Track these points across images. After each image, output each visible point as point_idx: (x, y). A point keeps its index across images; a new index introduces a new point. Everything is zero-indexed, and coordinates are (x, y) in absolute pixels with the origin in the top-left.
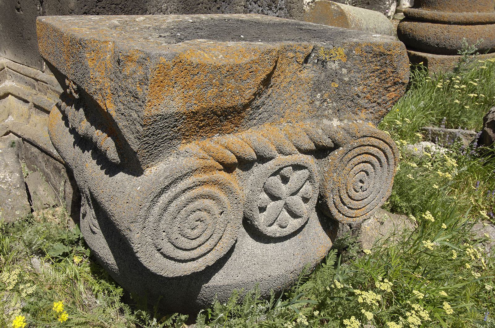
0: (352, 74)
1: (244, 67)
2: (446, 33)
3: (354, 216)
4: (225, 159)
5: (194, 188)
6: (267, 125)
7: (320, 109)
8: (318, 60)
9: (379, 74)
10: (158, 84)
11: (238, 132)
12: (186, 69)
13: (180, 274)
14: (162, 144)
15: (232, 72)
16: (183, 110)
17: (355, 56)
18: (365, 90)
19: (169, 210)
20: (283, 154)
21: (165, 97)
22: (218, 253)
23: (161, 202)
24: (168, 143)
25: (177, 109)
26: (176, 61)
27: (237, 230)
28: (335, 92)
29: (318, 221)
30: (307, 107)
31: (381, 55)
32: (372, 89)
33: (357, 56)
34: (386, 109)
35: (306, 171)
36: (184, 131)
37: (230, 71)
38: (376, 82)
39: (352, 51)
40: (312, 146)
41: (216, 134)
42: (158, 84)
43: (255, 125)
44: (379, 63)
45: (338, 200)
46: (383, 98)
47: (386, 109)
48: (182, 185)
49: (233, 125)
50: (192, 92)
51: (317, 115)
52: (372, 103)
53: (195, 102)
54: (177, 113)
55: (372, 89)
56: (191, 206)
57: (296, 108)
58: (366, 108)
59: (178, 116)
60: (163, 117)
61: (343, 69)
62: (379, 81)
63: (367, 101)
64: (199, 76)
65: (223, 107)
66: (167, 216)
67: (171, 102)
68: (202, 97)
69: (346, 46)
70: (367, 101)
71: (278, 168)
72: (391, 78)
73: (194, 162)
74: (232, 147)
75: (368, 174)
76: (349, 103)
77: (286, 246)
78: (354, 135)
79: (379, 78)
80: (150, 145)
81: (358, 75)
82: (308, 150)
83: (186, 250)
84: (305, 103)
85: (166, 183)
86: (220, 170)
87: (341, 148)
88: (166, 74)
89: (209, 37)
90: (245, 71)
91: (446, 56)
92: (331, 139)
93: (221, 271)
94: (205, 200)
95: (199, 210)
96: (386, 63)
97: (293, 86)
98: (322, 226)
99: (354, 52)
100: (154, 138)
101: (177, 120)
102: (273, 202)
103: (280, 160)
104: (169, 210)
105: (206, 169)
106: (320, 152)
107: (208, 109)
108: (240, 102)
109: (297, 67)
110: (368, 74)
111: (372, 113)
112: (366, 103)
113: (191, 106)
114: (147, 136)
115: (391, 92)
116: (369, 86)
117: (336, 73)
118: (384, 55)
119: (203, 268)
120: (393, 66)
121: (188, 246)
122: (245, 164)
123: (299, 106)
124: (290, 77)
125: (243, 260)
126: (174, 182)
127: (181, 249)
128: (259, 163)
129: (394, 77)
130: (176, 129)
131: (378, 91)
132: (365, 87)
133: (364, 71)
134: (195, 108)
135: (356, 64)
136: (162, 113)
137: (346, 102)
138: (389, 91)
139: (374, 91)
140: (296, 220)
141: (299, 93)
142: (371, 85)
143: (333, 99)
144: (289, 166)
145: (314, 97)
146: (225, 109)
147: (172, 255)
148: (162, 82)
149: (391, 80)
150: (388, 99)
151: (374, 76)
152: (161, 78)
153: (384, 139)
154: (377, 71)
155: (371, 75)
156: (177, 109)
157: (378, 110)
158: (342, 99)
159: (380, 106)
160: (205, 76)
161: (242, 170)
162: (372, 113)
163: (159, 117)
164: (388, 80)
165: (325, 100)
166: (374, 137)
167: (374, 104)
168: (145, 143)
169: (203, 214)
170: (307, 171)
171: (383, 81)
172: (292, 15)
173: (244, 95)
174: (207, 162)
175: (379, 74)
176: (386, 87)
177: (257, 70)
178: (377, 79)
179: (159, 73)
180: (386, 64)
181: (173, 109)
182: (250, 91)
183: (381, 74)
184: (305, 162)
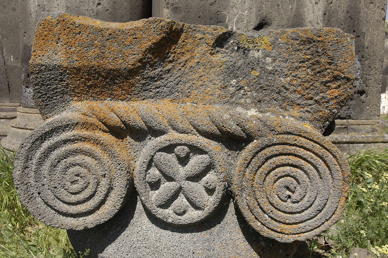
0: (277, 63)
1: (127, 32)
3: (279, 230)
4: (106, 119)
5: (76, 142)
6: (166, 101)
7: (235, 96)
8: (239, 48)
9: (310, 65)
10: (42, 37)
11: (132, 101)
12: (69, 28)
14: (54, 96)
16: (65, 64)
17: (281, 45)
18: (295, 82)
19: (51, 157)
20: (176, 130)
21: (49, 50)
22: (98, 218)
23: (44, 147)
24: (60, 96)
25: (60, 62)
26: (59, 20)
27: (120, 198)
28: (254, 81)
29: (238, 227)
30: (218, 92)
31: (311, 43)
32: (304, 82)
33: (283, 43)
34: (330, 110)
36: (72, 87)
37: (112, 34)
38: (308, 74)
39: (277, 39)
41: (108, 98)
42: (42, 37)
43: (151, 97)
44: (308, 52)
45: (253, 203)
46: (321, 94)
47: (330, 110)
48: (64, 136)
49: (124, 92)
50: (74, 49)
51: (231, 100)
52: (306, 99)
53: (76, 58)
55: (304, 82)
56: (71, 159)
57: (206, 91)
58: (299, 105)
59: (62, 70)
60: (48, 68)
61: (267, 58)
62: (312, 74)
63: (299, 96)
64: (81, 35)
65: (105, 68)
66: (48, 164)
67: (54, 55)
68: (83, 55)
69: (271, 35)
70: (299, 96)
71: (167, 143)
72: (329, 71)
74: (117, 110)
76: (275, 96)
77: (184, 239)
78: (273, 129)
79: (312, 70)
80: (42, 95)
81: (284, 65)
82: (208, 133)
84: (216, 86)
85: (46, 129)
86: (104, 131)
87: (255, 141)
88: (50, 30)
89: (128, 22)
90: (128, 37)
92: (241, 127)
93: (113, 244)
94: (86, 157)
95: (78, 164)
96: (317, 52)
97: (202, 68)
98: (244, 234)
99: (280, 40)
100: (44, 88)
101: (62, 73)
102: (168, 183)
103: (172, 136)
104: (51, 157)
105: (86, 125)
106: (234, 141)
107: (90, 68)
108: (123, 66)
109: (207, 49)
110: (296, 64)
111: (310, 112)
112: (299, 98)
113: (73, 62)
115: (332, 89)
116: (300, 78)
117: (259, 61)
118: (314, 42)
119: (82, 228)
120: (328, 55)
121: (67, 199)
123: (209, 89)
124: (198, 57)
125: (135, 239)
128: (152, 136)
129: (332, 69)
131: (314, 86)
132: (295, 79)
133: (291, 60)
134: (76, 64)
135: (282, 53)
136: (45, 64)
137: (268, 92)
138: (329, 86)
140: (197, 211)
141: (210, 76)
142: (301, 76)
143: (252, 88)
144: (185, 145)
145: (228, 82)
146: (108, 70)
147: (51, 203)
148: (46, 36)
149: (329, 73)
150: (329, 97)
151: (304, 67)
152: (46, 33)
153: (321, 143)
154: (308, 61)
155: (300, 65)
156: (60, 62)
157: (318, 109)
158: (264, 90)
159: (320, 105)
160: (87, 36)
161: (134, 140)
162: (310, 112)
163: (44, 67)
164: (325, 73)
165: (242, 87)
166: (305, 137)
167: (310, 102)
168: (38, 92)
169: (83, 170)
170: (208, 156)
171: (319, 74)
172: (369, 85)
173: (127, 60)
174: (88, 119)
175: (310, 65)
176: (323, 82)
177: (142, 38)
178: (309, 70)
179: (44, 28)
180: (318, 52)
181: (55, 62)
182: (134, 56)
183: (314, 64)
184: (203, 145)
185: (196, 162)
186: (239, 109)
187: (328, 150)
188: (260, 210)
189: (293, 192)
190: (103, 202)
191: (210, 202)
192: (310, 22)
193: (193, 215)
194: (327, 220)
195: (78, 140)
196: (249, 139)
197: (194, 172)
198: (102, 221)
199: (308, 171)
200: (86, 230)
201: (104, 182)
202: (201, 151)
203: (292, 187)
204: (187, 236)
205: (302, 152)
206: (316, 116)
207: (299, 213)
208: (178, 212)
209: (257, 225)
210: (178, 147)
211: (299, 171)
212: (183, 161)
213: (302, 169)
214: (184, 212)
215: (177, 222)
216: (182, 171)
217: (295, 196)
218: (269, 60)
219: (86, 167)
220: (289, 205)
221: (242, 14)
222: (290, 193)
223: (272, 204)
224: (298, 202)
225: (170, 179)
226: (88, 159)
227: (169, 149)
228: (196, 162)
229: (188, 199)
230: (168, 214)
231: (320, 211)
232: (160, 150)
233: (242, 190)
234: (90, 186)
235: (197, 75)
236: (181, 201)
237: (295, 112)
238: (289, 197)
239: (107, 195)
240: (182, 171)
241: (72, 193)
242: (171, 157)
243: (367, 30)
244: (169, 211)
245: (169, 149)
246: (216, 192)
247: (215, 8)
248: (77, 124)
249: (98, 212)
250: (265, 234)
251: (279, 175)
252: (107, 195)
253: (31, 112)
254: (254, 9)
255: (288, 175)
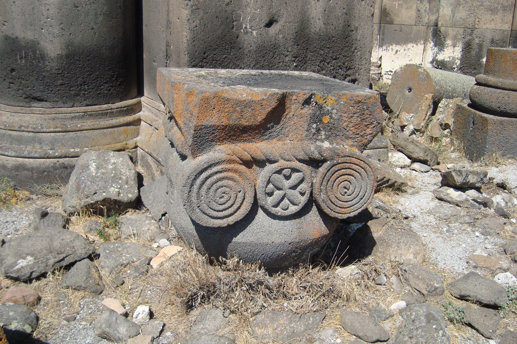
2: (506, 98)
13: (210, 225)
15: (248, 104)
16: (217, 124)
18: (349, 125)
22: (236, 218)
35: (300, 174)
40: (307, 158)
54: (214, 126)
56: (220, 183)
60: (206, 127)
66: (205, 187)
71: (279, 168)
73: (223, 156)
75: (350, 183)
83: (215, 210)
86: (241, 164)
87: (328, 162)
91: (508, 119)
97: (296, 118)
103: (282, 163)
105: (230, 161)
106: (315, 163)
110: (351, 115)
114: (196, 137)
119: (226, 225)
122: (261, 163)
126: (210, 166)
127: (212, 209)
130: (214, 135)
139: (357, 127)
144: (289, 168)
147: (207, 212)
167: (357, 136)
169: (227, 189)
185: (296, 177)
186: (318, 143)
187: (367, 164)
188: (330, 202)
189: (348, 190)
190: (239, 208)
191: (303, 200)
192: (313, 18)
193: (293, 209)
194: (365, 203)
195: (225, 171)
196: (325, 161)
197: (294, 184)
198: (239, 219)
199: (357, 177)
200: (229, 226)
201: (240, 195)
202: (298, 171)
203: (347, 187)
204: (287, 222)
205: (354, 167)
206: (360, 144)
207: (351, 201)
208: (284, 208)
209: (327, 211)
210: (285, 170)
211: (352, 177)
212: (288, 178)
213: (353, 176)
214: (287, 209)
215: (283, 215)
216: (287, 184)
217: (349, 192)
218: (335, 111)
219: (229, 187)
220: (347, 198)
221: (254, 13)
222: (346, 190)
223: (337, 198)
224: (350, 195)
225: (279, 189)
226: (230, 182)
227: (279, 172)
228: (296, 177)
229: (289, 200)
230: (278, 211)
231: (362, 199)
232: (275, 173)
233: (321, 191)
234: (232, 199)
235: (292, 122)
236: (286, 201)
237: (350, 142)
238: (346, 192)
239: (242, 203)
240: (287, 184)
241: (220, 205)
242: (281, 177)
243: (360, 25)
244: (278, 208)
245: (279, 172)
246: (306, 194)
247: (230, 8)
248: (225, 161)
249: (236, 214)
250: (332, 216)
251: (341, 181)
252: (242, 203)
253: (24, 112)
254: (265, 8)
255: (346, 181)
